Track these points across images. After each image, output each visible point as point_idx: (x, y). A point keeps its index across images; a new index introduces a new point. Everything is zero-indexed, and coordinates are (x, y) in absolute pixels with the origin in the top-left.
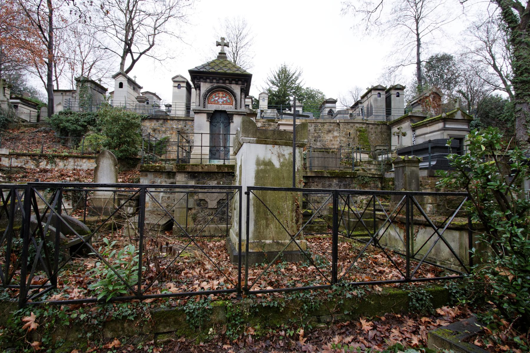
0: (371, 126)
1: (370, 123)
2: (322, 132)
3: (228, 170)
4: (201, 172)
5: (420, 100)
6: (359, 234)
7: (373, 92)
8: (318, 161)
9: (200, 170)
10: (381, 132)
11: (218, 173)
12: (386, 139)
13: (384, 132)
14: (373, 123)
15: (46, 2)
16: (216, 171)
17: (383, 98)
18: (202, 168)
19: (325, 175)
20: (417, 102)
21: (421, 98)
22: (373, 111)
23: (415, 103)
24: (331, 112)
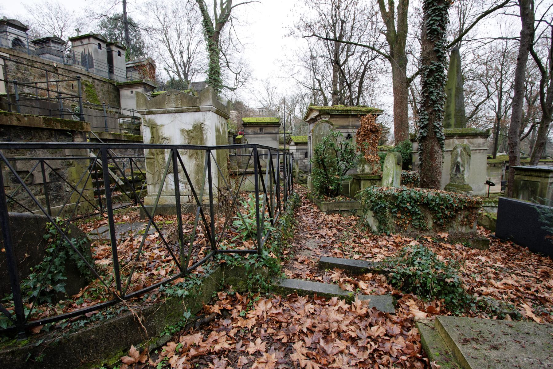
0: (97, 82)
1: (96, 78)
2: (31, 74)
3: (61, 127)
4: (17, 126)
5: (137, 66)
6: (411, 10)
7: (92, 40)
8: (97, 121)
9: (15, 123)
10: (108, 91)
11: (42, 129)
12: (114, 101)
13: (111, 92)
14: (99, 78)
15: (471, 363)
16: (44, 126)
17: (104, 51)
18: (19, 120)
19: (123, 139)
20: (133, 67)
21: (138, 64)
22: (94, 64)
23: (130, 67)
24: (17, 42)
